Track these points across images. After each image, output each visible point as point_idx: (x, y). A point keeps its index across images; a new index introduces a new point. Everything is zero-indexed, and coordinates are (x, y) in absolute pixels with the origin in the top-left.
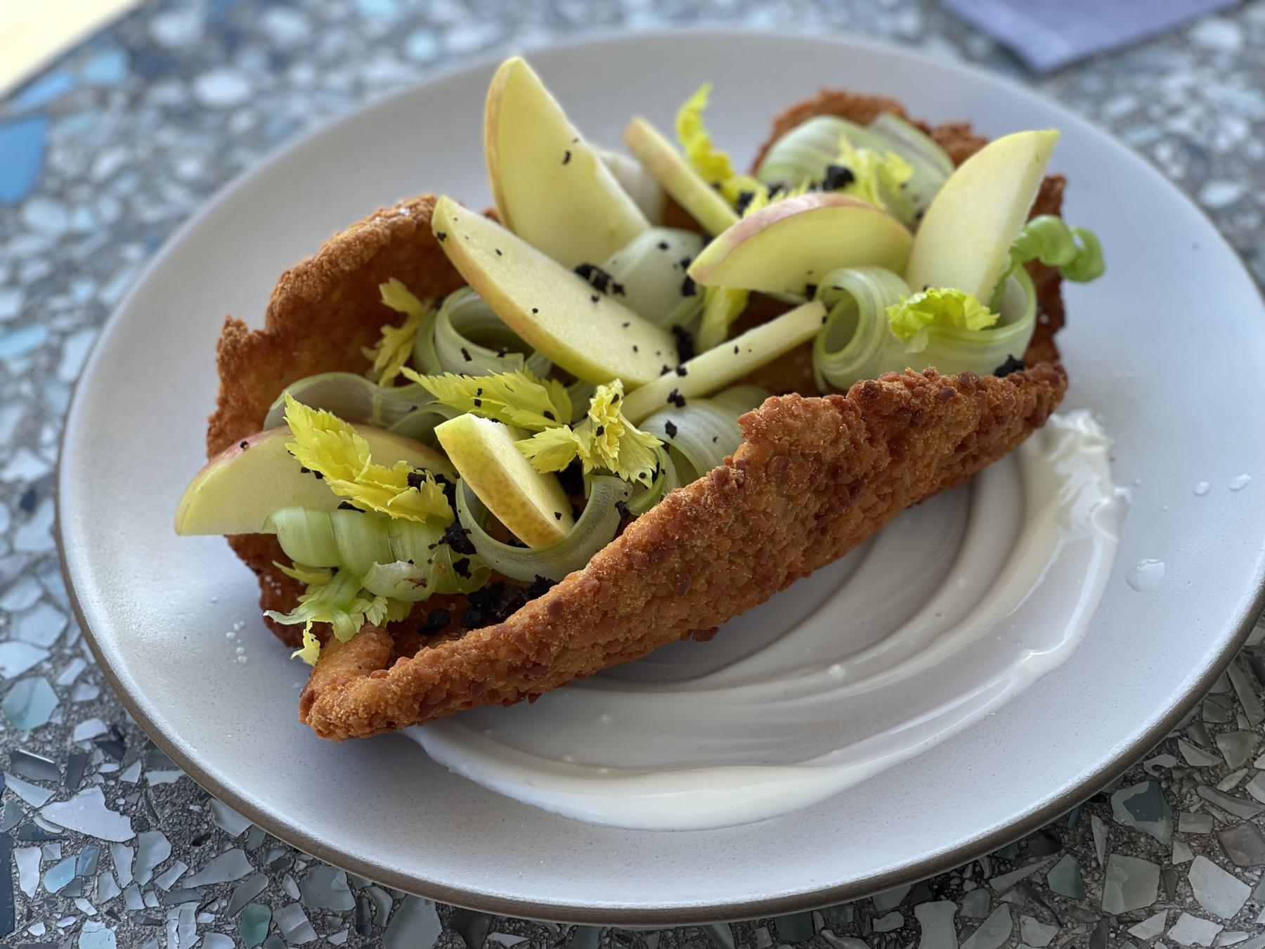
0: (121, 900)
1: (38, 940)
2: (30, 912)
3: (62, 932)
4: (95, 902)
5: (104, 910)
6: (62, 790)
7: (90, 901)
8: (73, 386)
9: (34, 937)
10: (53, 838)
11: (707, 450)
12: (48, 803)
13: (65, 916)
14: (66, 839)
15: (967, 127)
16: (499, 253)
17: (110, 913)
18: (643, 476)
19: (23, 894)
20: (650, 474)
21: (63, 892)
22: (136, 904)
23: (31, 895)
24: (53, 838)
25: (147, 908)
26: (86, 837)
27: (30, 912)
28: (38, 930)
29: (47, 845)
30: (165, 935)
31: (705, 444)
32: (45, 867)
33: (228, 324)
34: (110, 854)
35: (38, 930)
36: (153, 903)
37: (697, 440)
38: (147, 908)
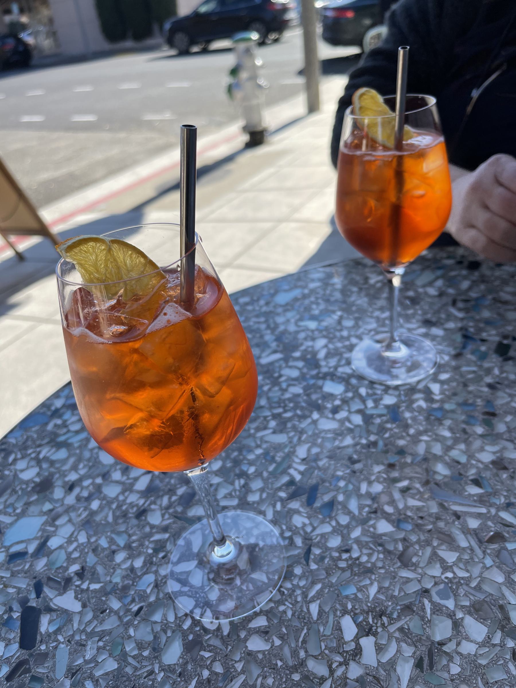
2: (42, 639)
3: (51, 648)
5: (67, 639)
7: (63, 636)
14: (59, 611)
19: (41, 633)
26: (66, 610)
35: (43, 647)
36: (84, 637)
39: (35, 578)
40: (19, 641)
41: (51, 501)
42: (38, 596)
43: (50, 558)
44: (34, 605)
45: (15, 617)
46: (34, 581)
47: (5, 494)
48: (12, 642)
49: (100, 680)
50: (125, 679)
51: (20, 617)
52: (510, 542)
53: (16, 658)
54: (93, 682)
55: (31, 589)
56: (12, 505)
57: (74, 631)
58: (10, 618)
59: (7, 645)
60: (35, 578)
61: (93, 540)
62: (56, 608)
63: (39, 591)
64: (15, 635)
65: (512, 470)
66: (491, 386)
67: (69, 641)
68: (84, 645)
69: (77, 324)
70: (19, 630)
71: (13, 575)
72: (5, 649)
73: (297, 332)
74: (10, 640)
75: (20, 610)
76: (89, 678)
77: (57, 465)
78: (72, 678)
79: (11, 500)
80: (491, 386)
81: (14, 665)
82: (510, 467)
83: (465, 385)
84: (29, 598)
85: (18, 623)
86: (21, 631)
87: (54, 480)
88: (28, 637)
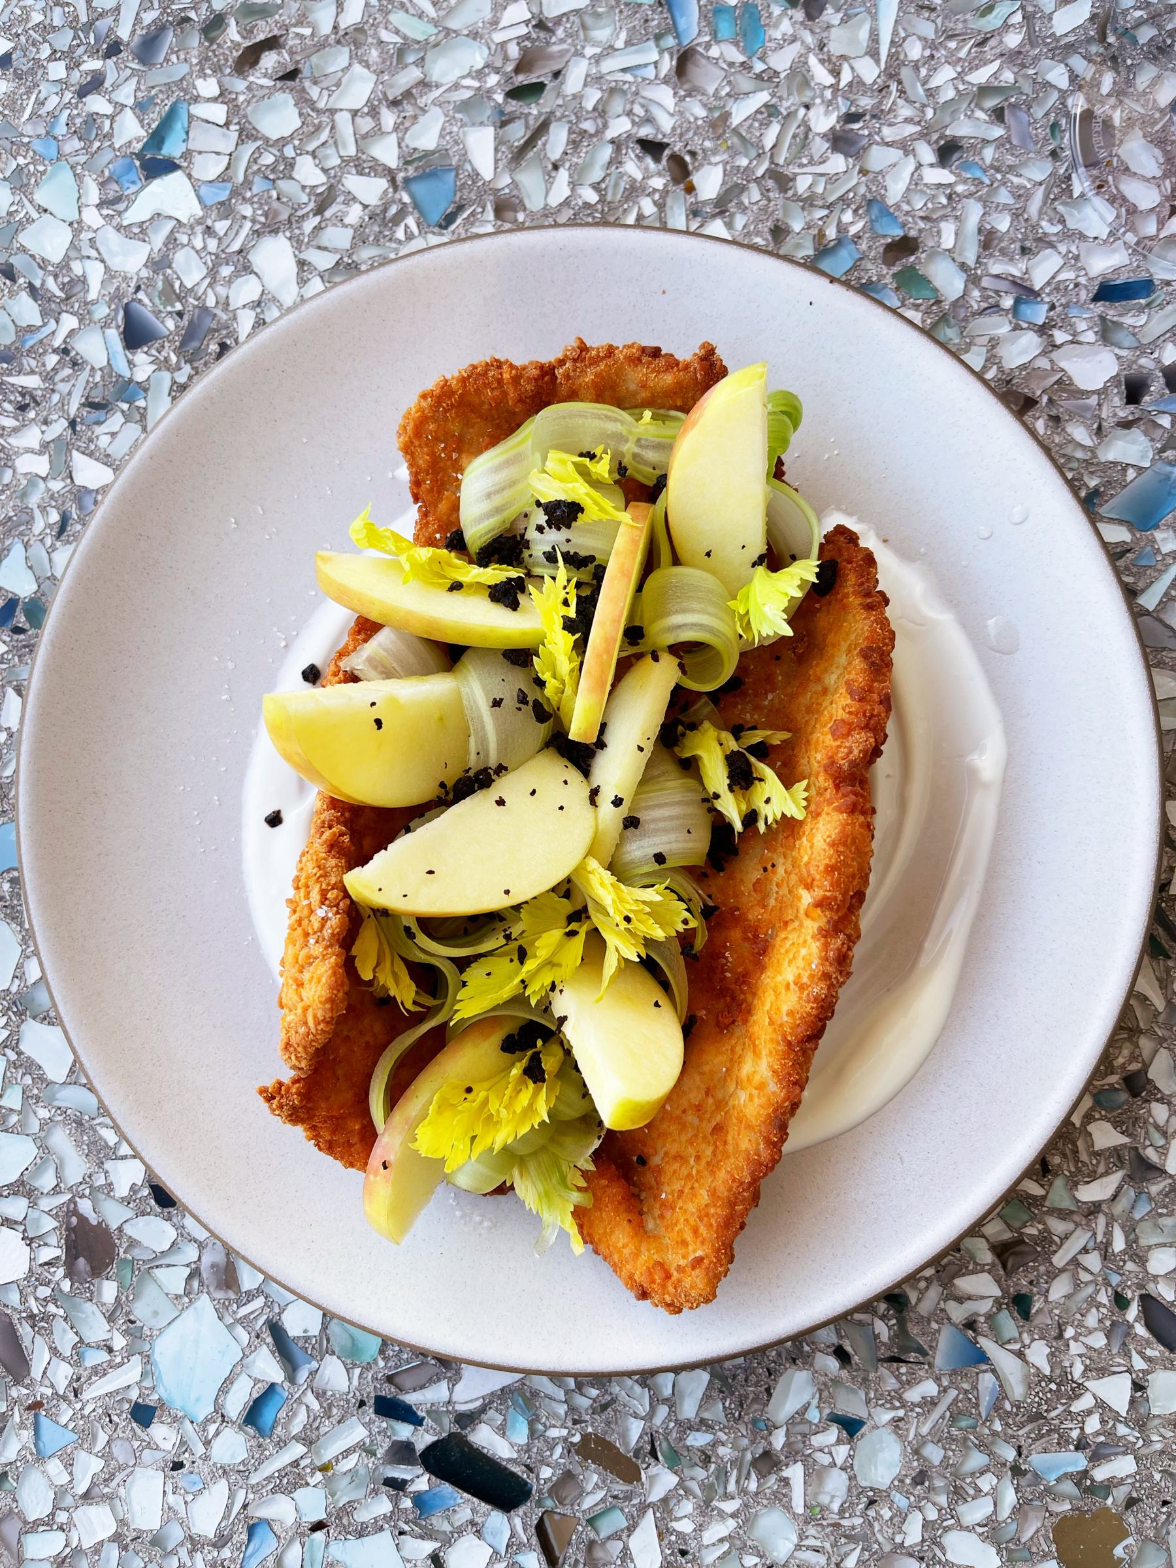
0: (572, 1409)
1: (554, 1479)
2: (527, 1466)
3: (562, 1461)
4: (558, 1424)
5: (570, 1424)
6: (449, 1375)
7: (555, 1426)
8: (76, 1068)
9: (550, 1479)
10: (483, 1410)
11: (691, 845)
12: (451, 1391)
13: (552, 1449)
14: (491, 1402)
15: (583, 348)
16: (431, 872)
17: (575, 1422)
18: (685, 922)
19: (509, 1460)
20: (687, 915)
21: (532, 1433)
22: (583, 1402)
23: (515, 1456)
24: (483, 1410)
25: (594, 1400)
26: (502, 1390)
27: (527, 1466)
28: (546, 1472)
29: (484, 1417)
30: (625, 1406)
31: (685, 841)
32: (502, 1430)
33: (270, 1099)
34: (531, 1388)
35: (546, 1472)
36: (594, 1392)
37: (680, 845)
38: (594, 1400)
39: (362, 1404)
40: (490, 1507)
41: (157, 1260)
42: (417, 1422)
43: (337, 1350)
44: (429, 1439)
45: (425, 1487)
46: (370, 1410)
47: (26, 1342)
48: (478, 1520)
49: (706, 1415)
50: (741, 1377)
51: (433, 1478)
52: (1143, 591)
53: (525, 1530)
54: (698, 1430)
55: (384, 1425)
56: (81, 1344)
57: (566, 1402)
58: (419, 1500)
59: (479, 1533)
60: (362, 1404)
61: (374, 55)
62: (478, 1404)
63: (407, 1414)
64: (465, 1506)
65: (1045, 399)
66: (840, 141)
67: (575, 1422)
68: (614, 1401)
69: (620, 971)
70: (465, 1494)
71: (308, 1439)
72: (484, 1540)
73: (159, 264)
74: (472, 1523)
75: (419, 1470)
76: (684, 1432)
77: (47, 1181)
78: (657, 1459)
79: (66, 1340)
80: (840, 141)
81: (535, 1540)
82: (1038, 393)
83: (784, 182)
84: (404, 1439)
85: (447, 1488)
86: (469, 1492)
87: (93, 1220)
88: (499, 1488)
